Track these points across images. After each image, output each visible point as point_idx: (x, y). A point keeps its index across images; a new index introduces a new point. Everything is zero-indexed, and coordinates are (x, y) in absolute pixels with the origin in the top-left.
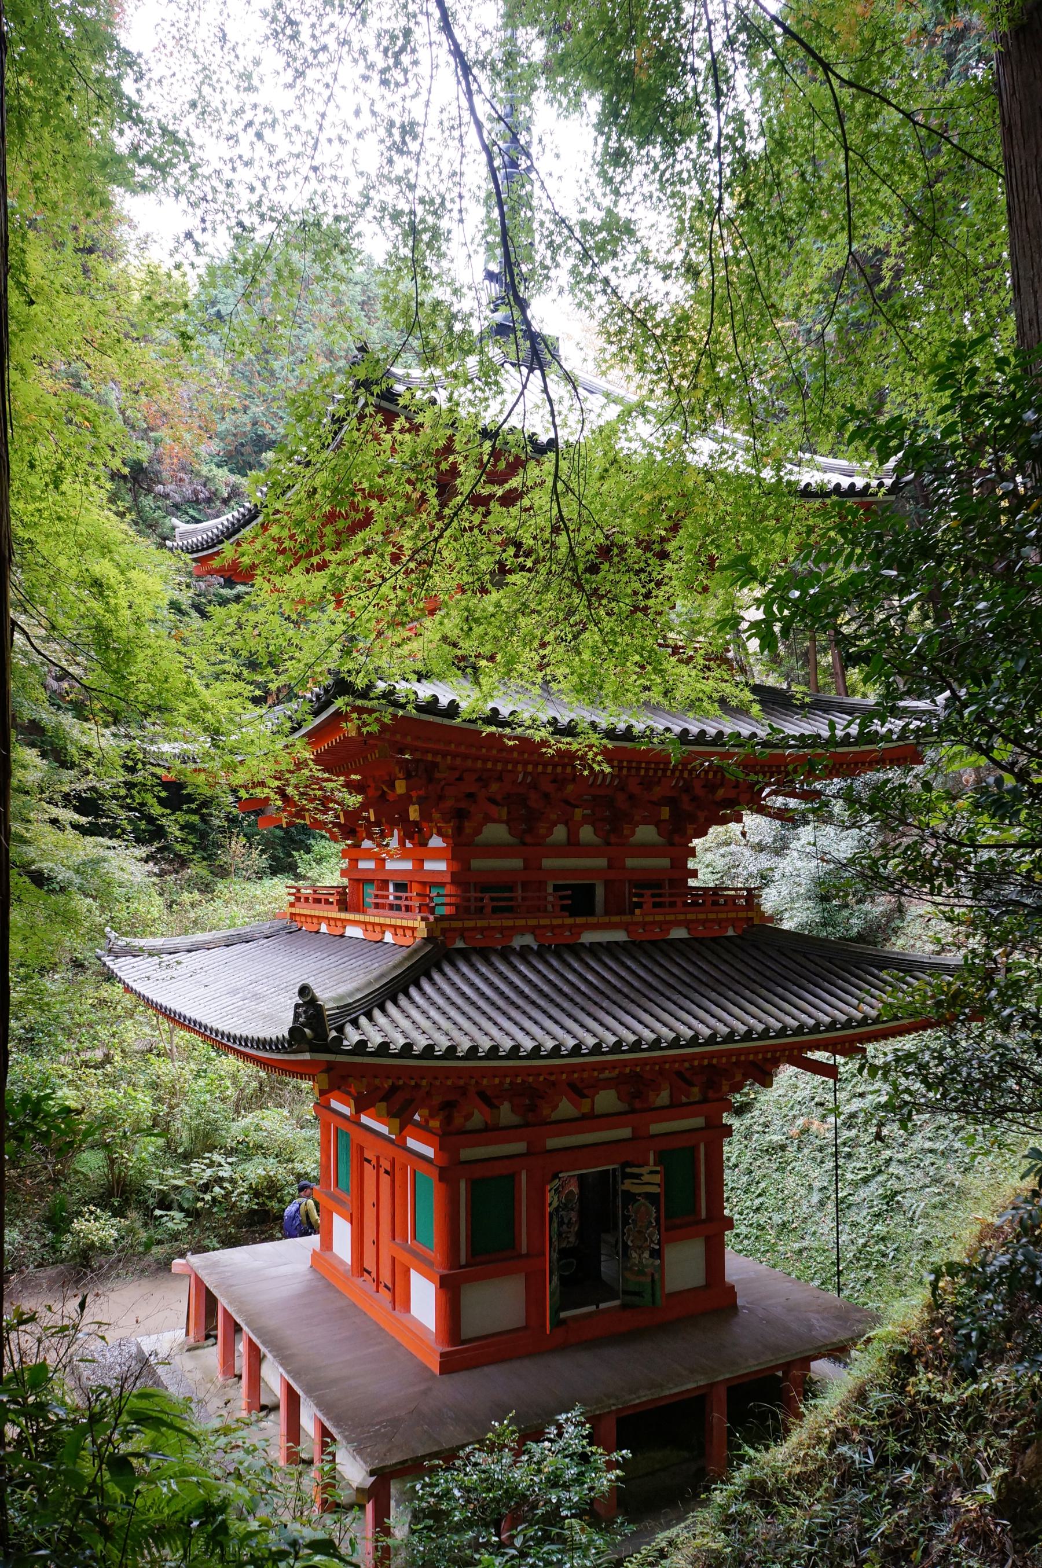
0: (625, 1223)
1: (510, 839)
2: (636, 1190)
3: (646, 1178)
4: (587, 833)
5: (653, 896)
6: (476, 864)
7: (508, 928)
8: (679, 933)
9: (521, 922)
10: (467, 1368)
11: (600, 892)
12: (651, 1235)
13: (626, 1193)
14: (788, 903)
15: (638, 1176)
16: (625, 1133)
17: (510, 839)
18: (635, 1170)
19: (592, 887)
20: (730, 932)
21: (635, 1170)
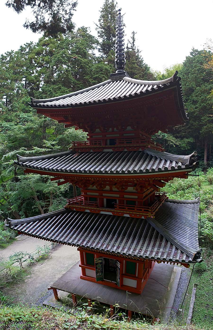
20: (143, 218)
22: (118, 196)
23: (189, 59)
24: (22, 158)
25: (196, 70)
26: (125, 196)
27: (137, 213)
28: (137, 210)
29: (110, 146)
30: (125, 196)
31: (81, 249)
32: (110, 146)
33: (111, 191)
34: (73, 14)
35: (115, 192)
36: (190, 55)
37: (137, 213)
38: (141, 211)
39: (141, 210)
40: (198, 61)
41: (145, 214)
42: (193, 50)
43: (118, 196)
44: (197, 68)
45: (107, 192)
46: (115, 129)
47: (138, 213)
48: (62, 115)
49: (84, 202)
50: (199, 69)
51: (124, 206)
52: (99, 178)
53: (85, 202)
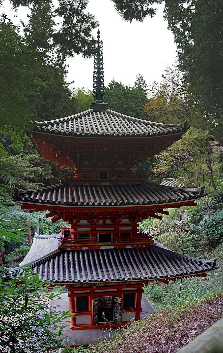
0: (115, 308)
1: (88, 223)
2: (117, 302)
3: (119, 300)
4: (108, 221)
5: (89, 239)
6: (78, 229)
7: (100, 245)
8: (97, 247)
9: (129, 243)
10: (89, 329)
11: (112, 235)
12: (119, 311)
13: (115, 302)
14: (162, 241)
15: (117, 299)
16: (116, 290)
17: (88, 223)
18: (117, 298)
19: (110, 235)
20: (144, 247)
21: (117, 298)
22: (113, 229)
23: (108, 91)
24: (20, 190)
25: (114, 104)
26: (120, 228)
27: (134, 243)
28: (139, 240)
29: (100, 179)
30: (120, 228)
31: (72, 288)
32: (100, 179)
33: (105, 225)
34: (52, 1)
35: (109, 226)
36: (108, 87)
37: (134, 243)
38: (136, 241)
39: (143, 240)
40: (117, 95)
41: (132, 243)
42: (113, 81)
43: (113, 229)
44: (116, 102)
45: (100, 226)
46: (106, 162)
47: (135, 243)
48: (160, 143)
49: (90, 239)
50: (117, 103)
51: (89, 241)
52: (154, 208)
53: (91, 238)
